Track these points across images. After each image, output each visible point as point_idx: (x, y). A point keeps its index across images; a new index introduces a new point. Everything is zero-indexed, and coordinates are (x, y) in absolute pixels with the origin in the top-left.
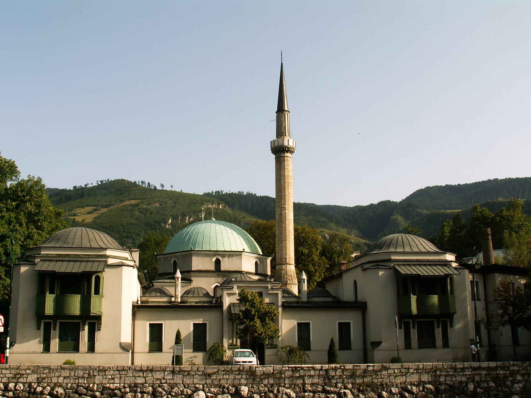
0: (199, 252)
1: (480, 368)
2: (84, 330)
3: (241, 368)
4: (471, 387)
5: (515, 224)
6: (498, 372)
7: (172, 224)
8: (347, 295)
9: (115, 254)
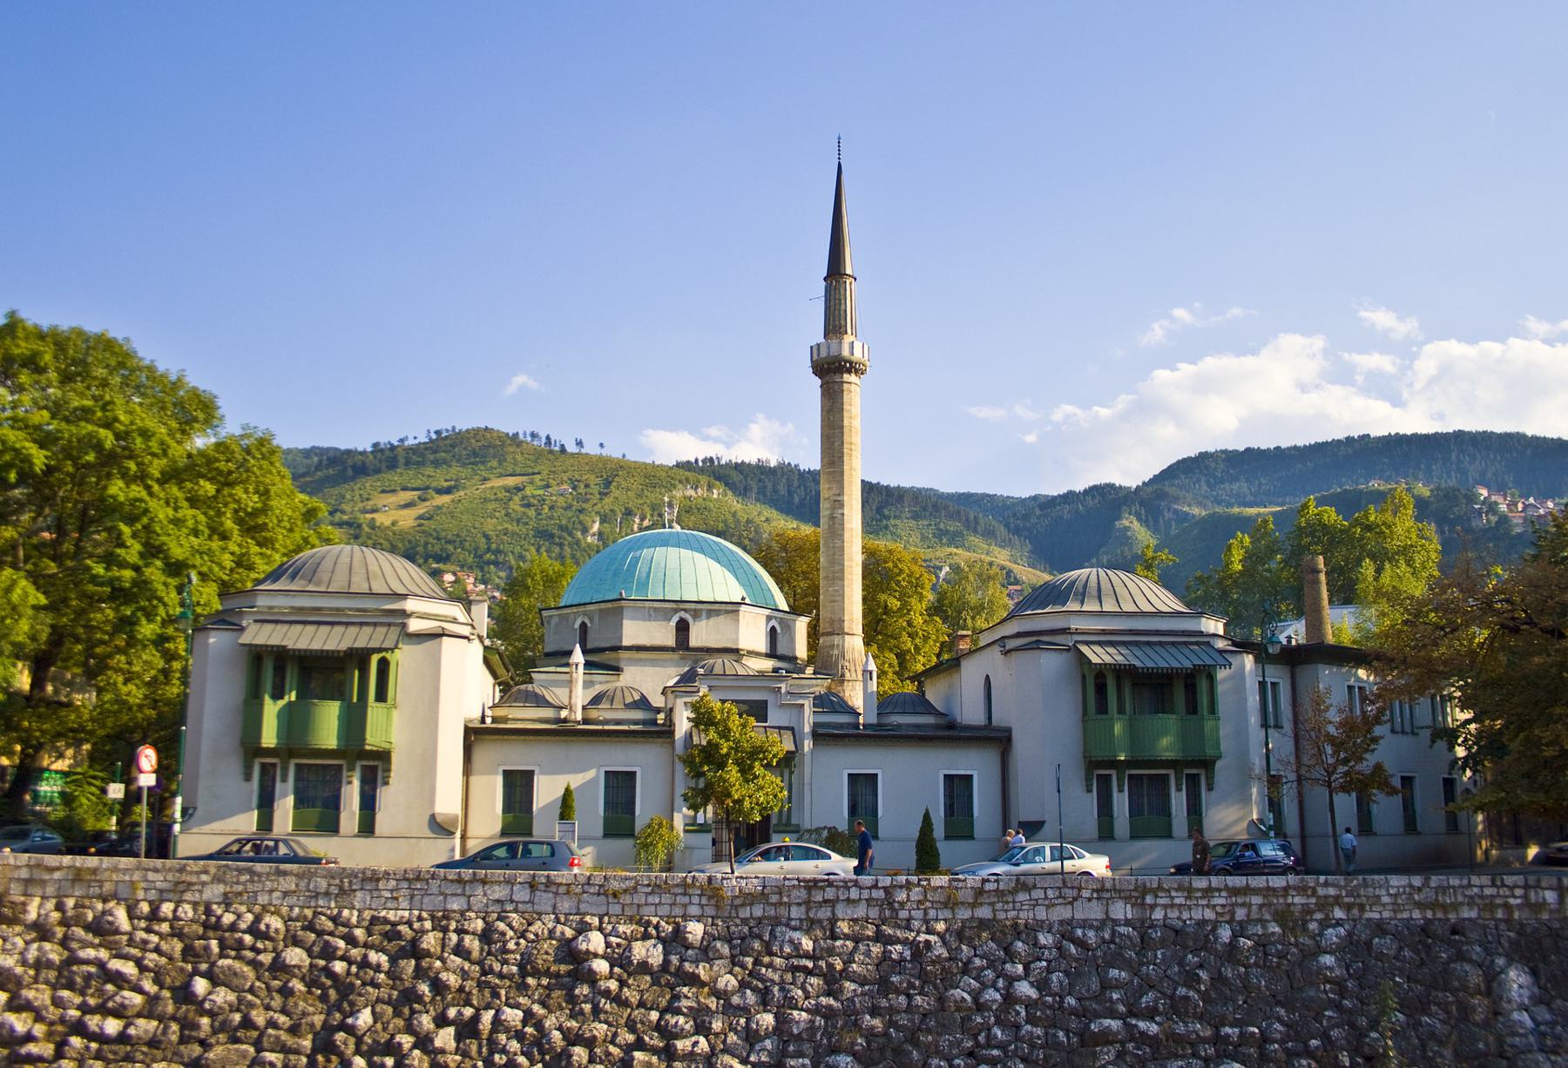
0: (639, 604)
1: (1247, 890)
2: (350, 783)
3: (689, 881)
4: (1225, 934)
5: (1394, 544)
6: (1290, 900)
7: (600, 534)
8: (970, 712)
9: (426, 609)
